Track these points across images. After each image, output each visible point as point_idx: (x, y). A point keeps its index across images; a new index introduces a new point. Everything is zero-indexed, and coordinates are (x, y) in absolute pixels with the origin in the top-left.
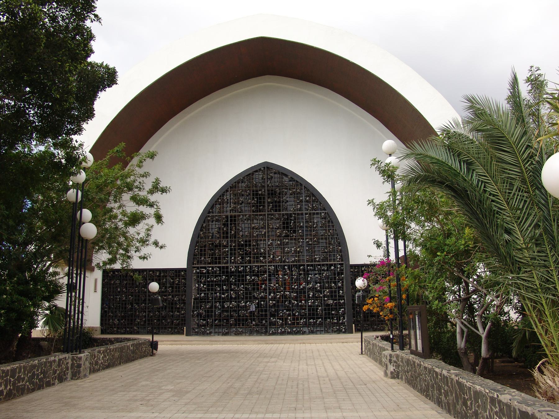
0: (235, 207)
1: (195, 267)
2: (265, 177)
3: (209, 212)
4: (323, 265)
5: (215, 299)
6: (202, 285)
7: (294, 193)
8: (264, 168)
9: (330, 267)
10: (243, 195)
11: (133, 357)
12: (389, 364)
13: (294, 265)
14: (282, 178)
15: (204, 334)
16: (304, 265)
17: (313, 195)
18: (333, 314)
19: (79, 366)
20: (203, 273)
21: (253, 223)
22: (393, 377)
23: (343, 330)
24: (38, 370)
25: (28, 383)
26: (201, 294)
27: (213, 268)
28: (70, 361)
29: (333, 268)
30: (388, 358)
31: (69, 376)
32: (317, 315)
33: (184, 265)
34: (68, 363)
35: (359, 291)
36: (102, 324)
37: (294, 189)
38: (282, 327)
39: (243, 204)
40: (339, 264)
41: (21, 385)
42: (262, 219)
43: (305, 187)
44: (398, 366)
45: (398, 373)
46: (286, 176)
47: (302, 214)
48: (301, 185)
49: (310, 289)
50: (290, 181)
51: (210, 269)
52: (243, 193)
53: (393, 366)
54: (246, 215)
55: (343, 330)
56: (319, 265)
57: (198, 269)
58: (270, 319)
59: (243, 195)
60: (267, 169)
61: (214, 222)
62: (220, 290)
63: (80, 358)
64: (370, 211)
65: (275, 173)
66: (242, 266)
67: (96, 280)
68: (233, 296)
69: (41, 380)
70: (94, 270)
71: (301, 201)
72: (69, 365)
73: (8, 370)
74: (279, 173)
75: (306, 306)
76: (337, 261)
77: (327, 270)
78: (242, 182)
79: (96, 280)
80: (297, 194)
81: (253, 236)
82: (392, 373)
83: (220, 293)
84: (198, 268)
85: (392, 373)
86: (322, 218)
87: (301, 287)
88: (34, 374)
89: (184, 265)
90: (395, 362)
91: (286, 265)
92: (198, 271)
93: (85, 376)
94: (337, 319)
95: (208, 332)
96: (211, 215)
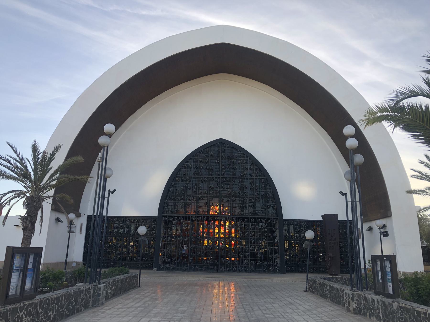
0: (197, 171)
1: (163, 216)
2: (220, 149)
3: (177, 174)
4: (262, 218)
5: (179, 241)
6: (169, 230)
7: (241, 163)
8: (220, 143)
9: (268, 220)
10: (203, 163)
11: (128, 288)
12: (351, 302)
13: (240, 218)
14: (233, 151)
15: (169, 270)
16: (248, 218)
17: (256, 165)
18: (269, 258)
19: (99, 295)
20: (170, 221)
21: (210, 184)
22: (355, 313)
23: (278, 271)
24: (72, 299)
25: (66, 310)
26: (168, 237)
27: (178, 218)
28: (92, 291)
29: (270, 221)
30: (351, 296)
31: (91, 303)
32: (257, 257)
33: (156, 215)
34: (91, 293)
35: (308, 240)
36: (83, 260)
37: (242, 159)
38: (230, 267)
39: (203, 170)
40: (275, 218)
41: (61, 311)
42: (217, 182)
43: (250, 159)
44: (360, 304)
45: (360, 310)
46: (236, 149)
47: (247, 178)
48: (247, 157)
49: (252, 236)
50: (239, 153)
51: (176, 217)
52: (203, 161)
53: (356, 303)
54: (205, 178)
55: (278, 271)
56: (260, 218)
57: (166, 217)
58: (221, 259)
59: (203, 163)
60: (221, 144)
61: (180, 182)
62: (183, 235)
63: (100, 288)
64: (419, 163)
65: (228, 147)
66: (200, 217)
67: (82, 224)
68: (193, 240)
69: (74, 307)
70: (80, 216)
71: (247, 169)
72: (91, 294)
73: (55, 298)
74: (231, 147)
75: (248, 250)
76: (273, 216)
77: (266, 223)
78: (203, 153)
79: (82, 224)
80: (244, 164)
81: (210, 193)
82: (354, 309)
83: (183, 237)
84: (166, 217)
85: (354, 309)
86: (262, 183)
87: (246, 235)
88: (70, 302)
89: (156, 215)
90: (357, 300)
91: (234, 217)
92: (166, 219)
93: (102, 304)
94: (273, 262)
95: (172, 268)
96: (178, 176)
